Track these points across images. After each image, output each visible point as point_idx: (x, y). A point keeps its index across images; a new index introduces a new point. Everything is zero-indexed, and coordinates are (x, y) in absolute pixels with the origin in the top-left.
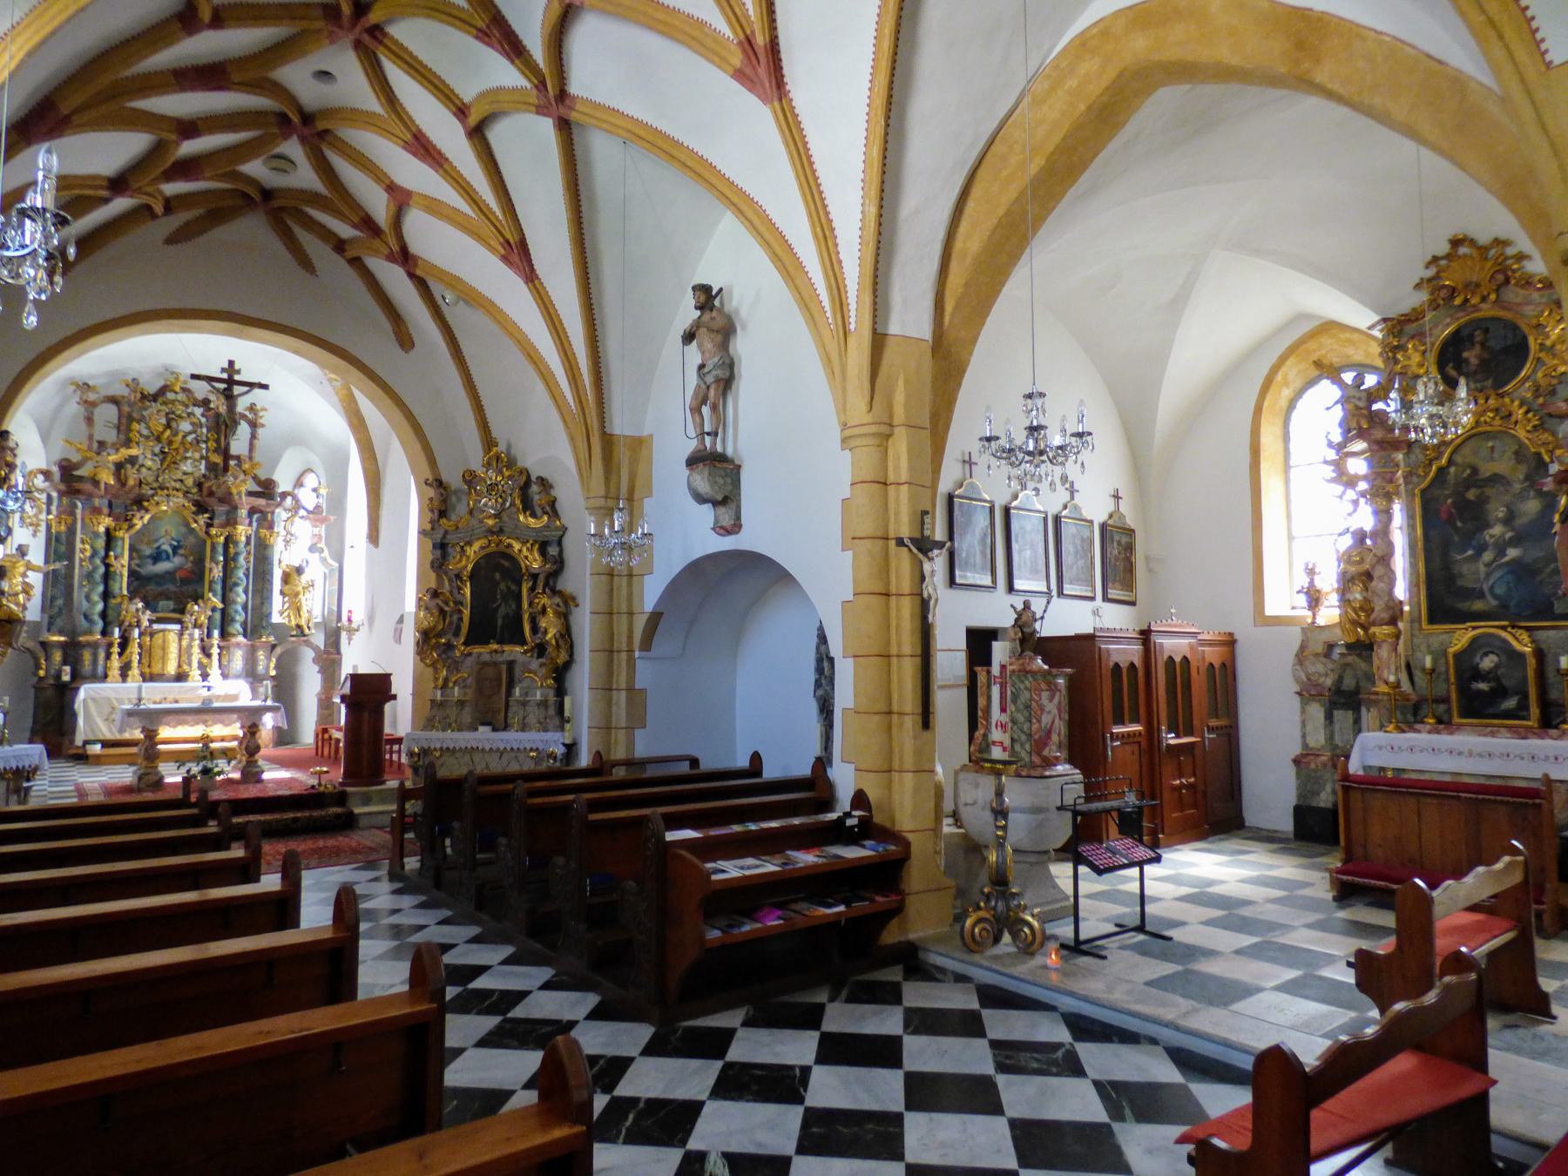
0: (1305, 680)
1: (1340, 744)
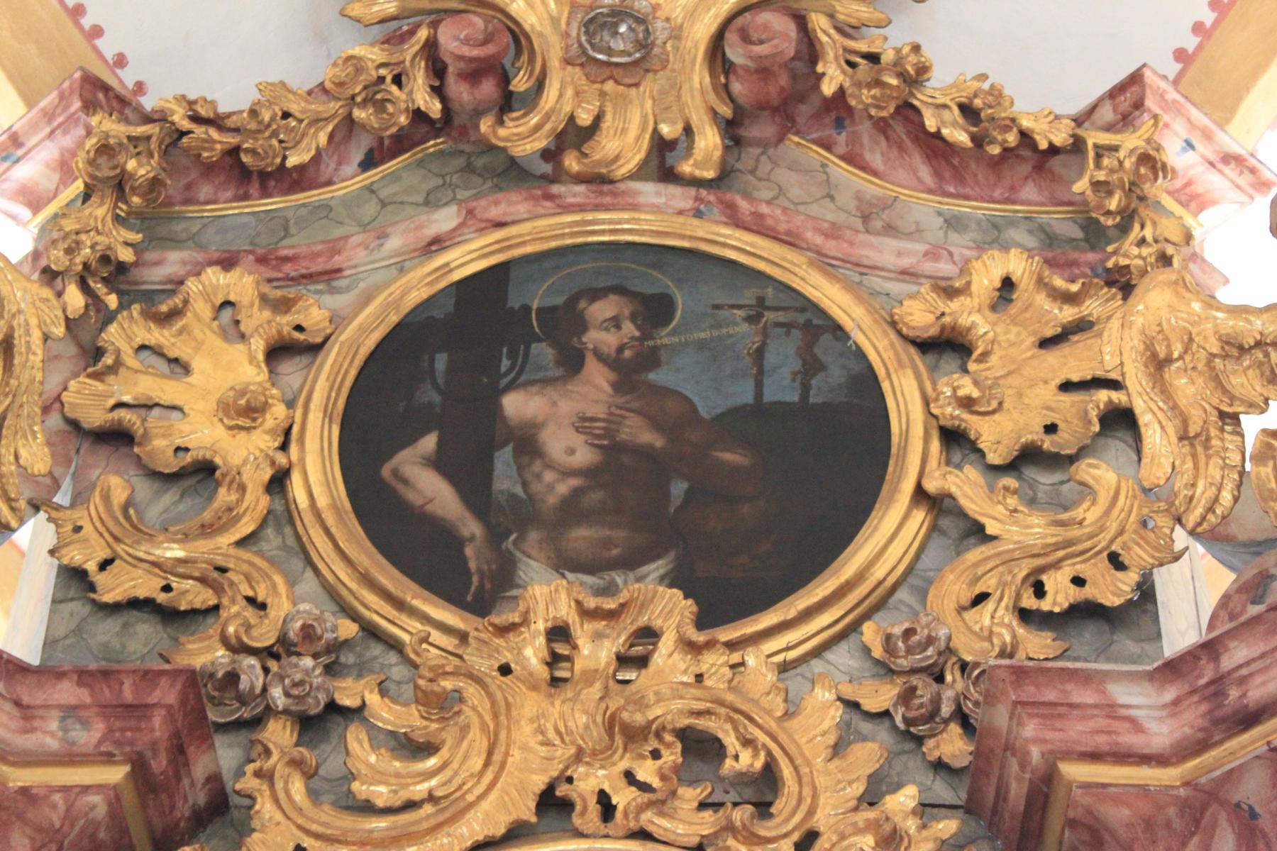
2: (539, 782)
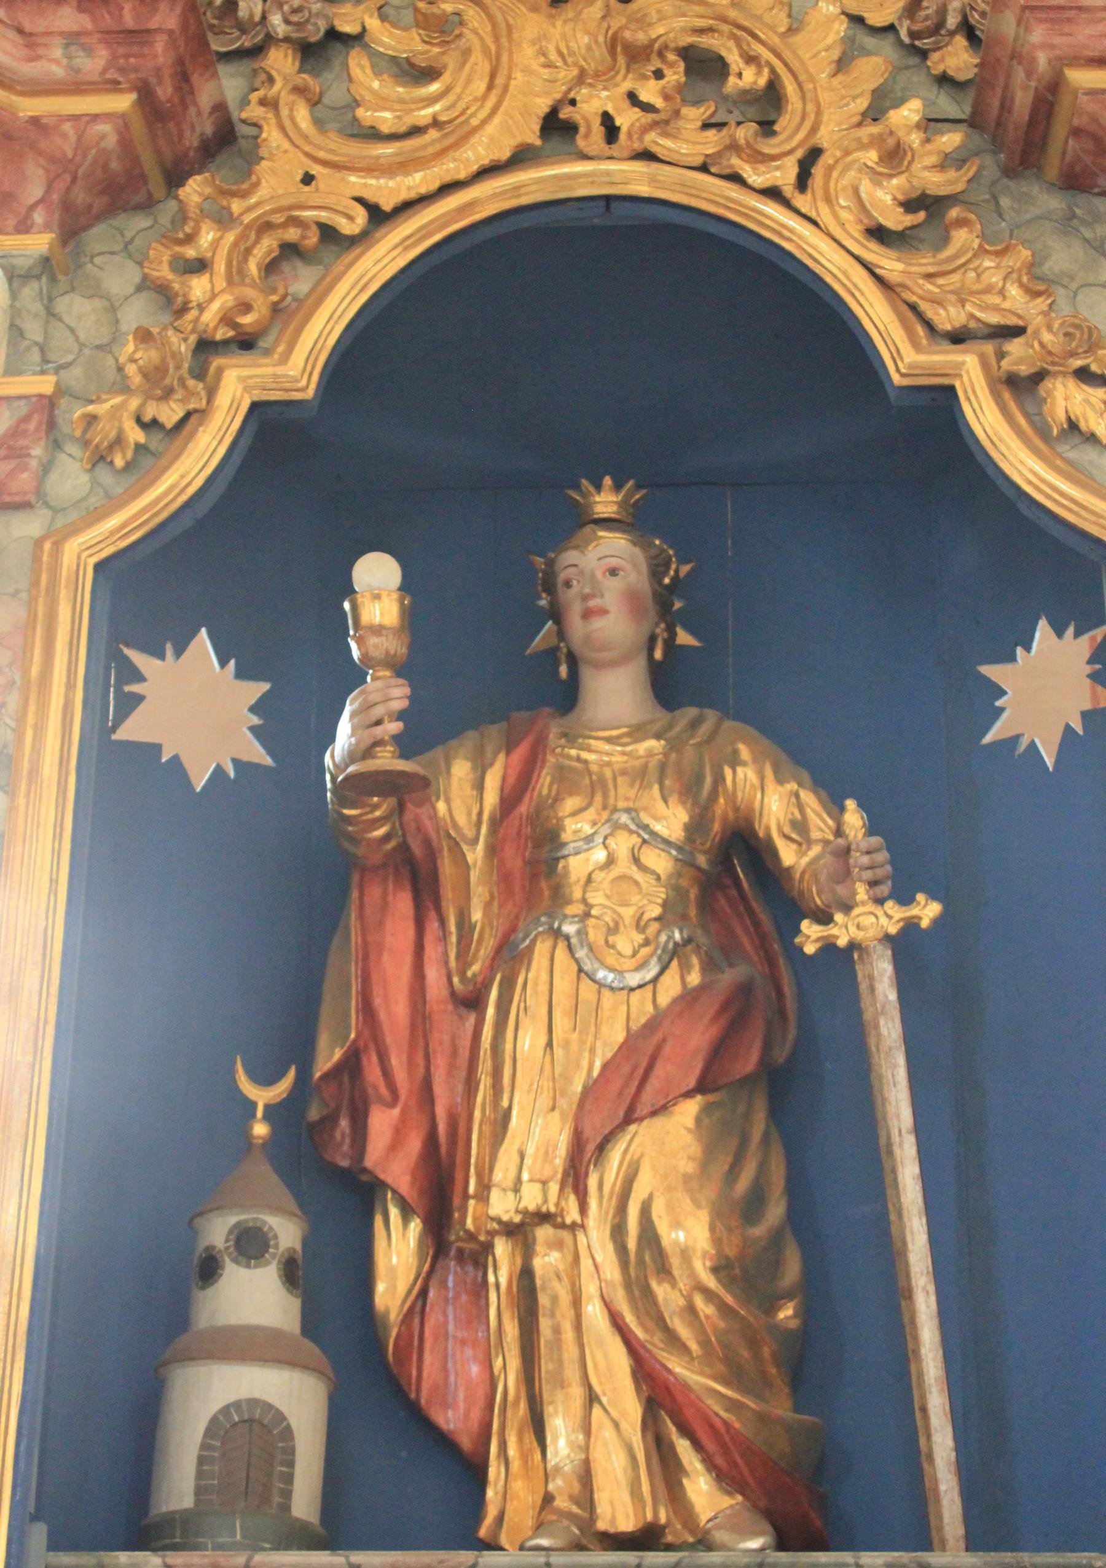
2: (543, 105)
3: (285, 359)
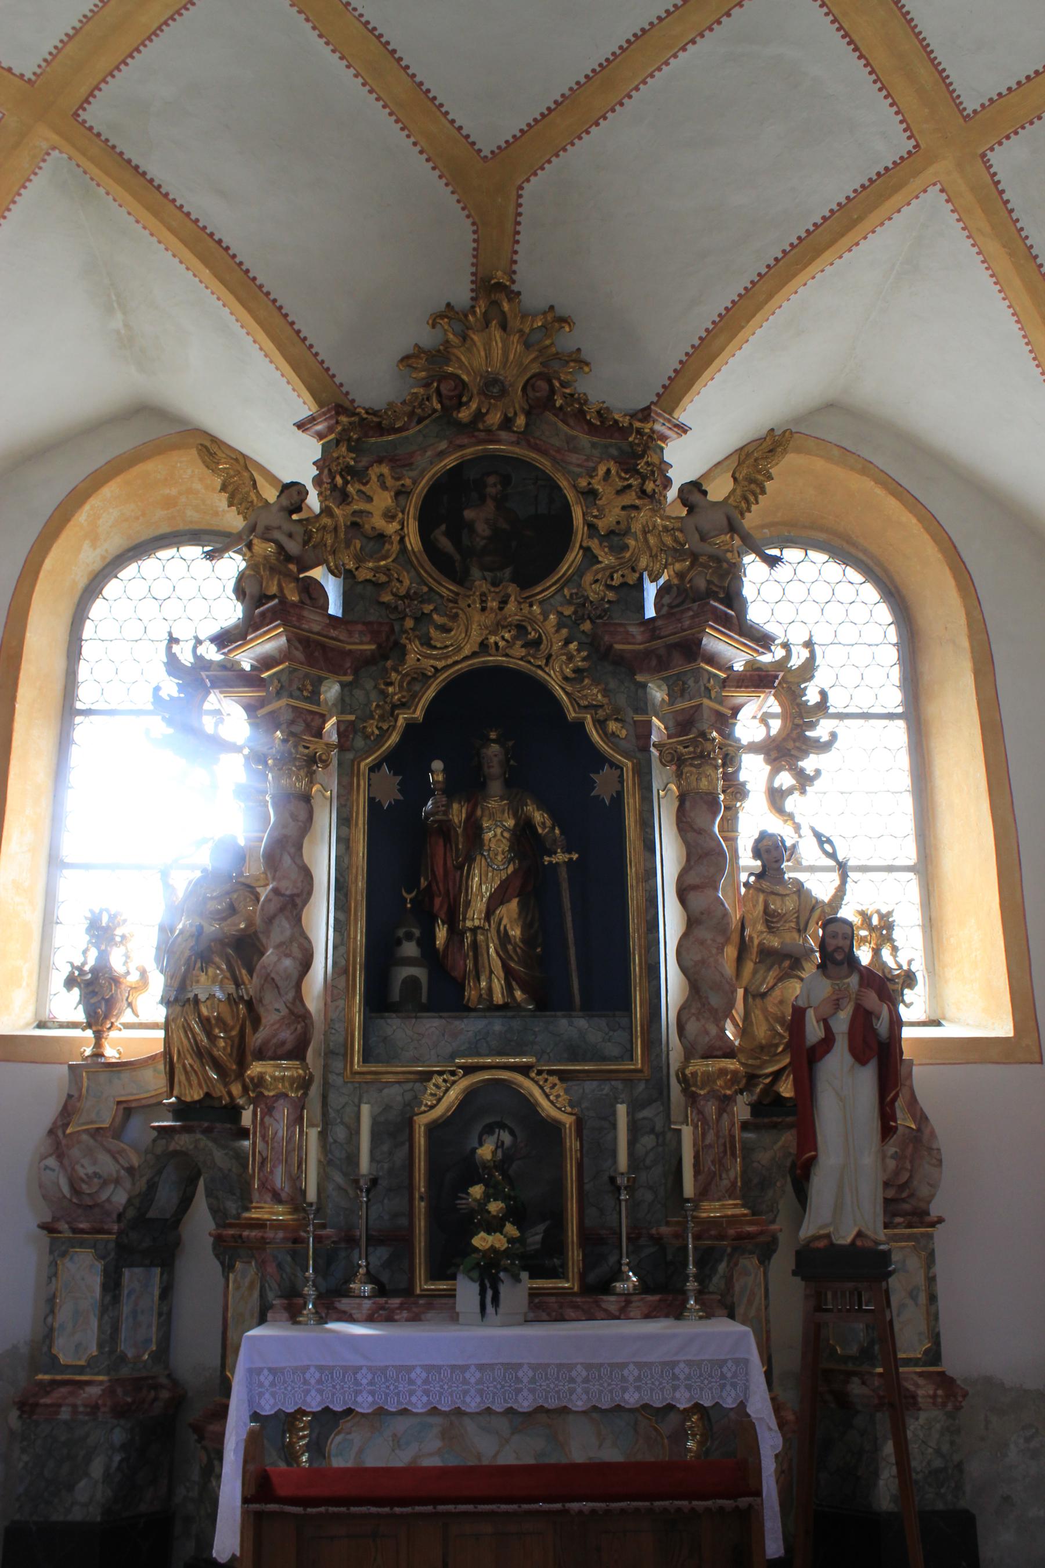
0: (66, 1190)
1: (130, 1354)
2: (479, 640)
3: (414, 712)
